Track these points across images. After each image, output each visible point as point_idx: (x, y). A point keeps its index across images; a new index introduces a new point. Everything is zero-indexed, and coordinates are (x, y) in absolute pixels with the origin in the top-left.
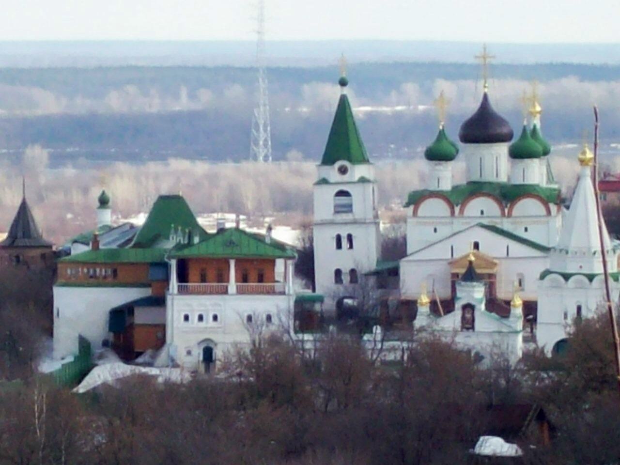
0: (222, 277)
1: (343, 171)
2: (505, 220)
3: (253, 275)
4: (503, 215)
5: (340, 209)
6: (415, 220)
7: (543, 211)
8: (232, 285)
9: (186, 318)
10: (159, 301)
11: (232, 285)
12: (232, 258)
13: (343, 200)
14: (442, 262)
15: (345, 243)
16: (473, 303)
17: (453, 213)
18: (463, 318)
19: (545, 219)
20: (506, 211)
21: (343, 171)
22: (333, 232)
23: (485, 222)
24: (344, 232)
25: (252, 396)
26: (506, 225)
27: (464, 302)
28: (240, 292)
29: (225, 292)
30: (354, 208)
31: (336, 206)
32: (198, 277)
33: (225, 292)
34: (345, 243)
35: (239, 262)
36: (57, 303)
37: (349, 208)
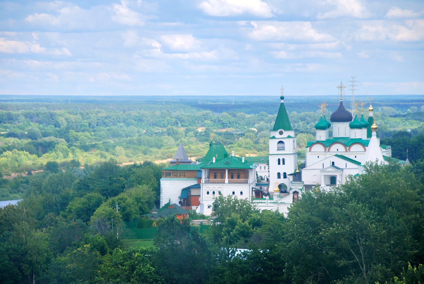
0: (223, 177)
1: (281, 133)
2: (346, 153)
3: (235, 175)
4: (346, 151)
5: (279, 149)
6: (310, 153)
7: (363, 150)
8: (227, 180)
9: (208, 193)
10: (198, 186)
11: (227, 180)
12: (227, 169)
13: (281, 145)
14: (319, 170)
15: (281, 162)
16: (298, 191)
17: (325, 150)
18: (294, 198)
19: (364, 153)
20: (327, 150)
21: (281, 133)
22: (277, 157)
23: (339, 154)
24: (281, 158)
25: (6, 221)
26: (347, 155)
27: (294, 190)
28: (229, 182)
29: (224, 183)
30: (285, 148)
31: (278, 147)
32: (213, 177)
33: (224, 183)
34: (281, 162)
35: (229, 170)
36: (162, 186)
37: (283, 149)
